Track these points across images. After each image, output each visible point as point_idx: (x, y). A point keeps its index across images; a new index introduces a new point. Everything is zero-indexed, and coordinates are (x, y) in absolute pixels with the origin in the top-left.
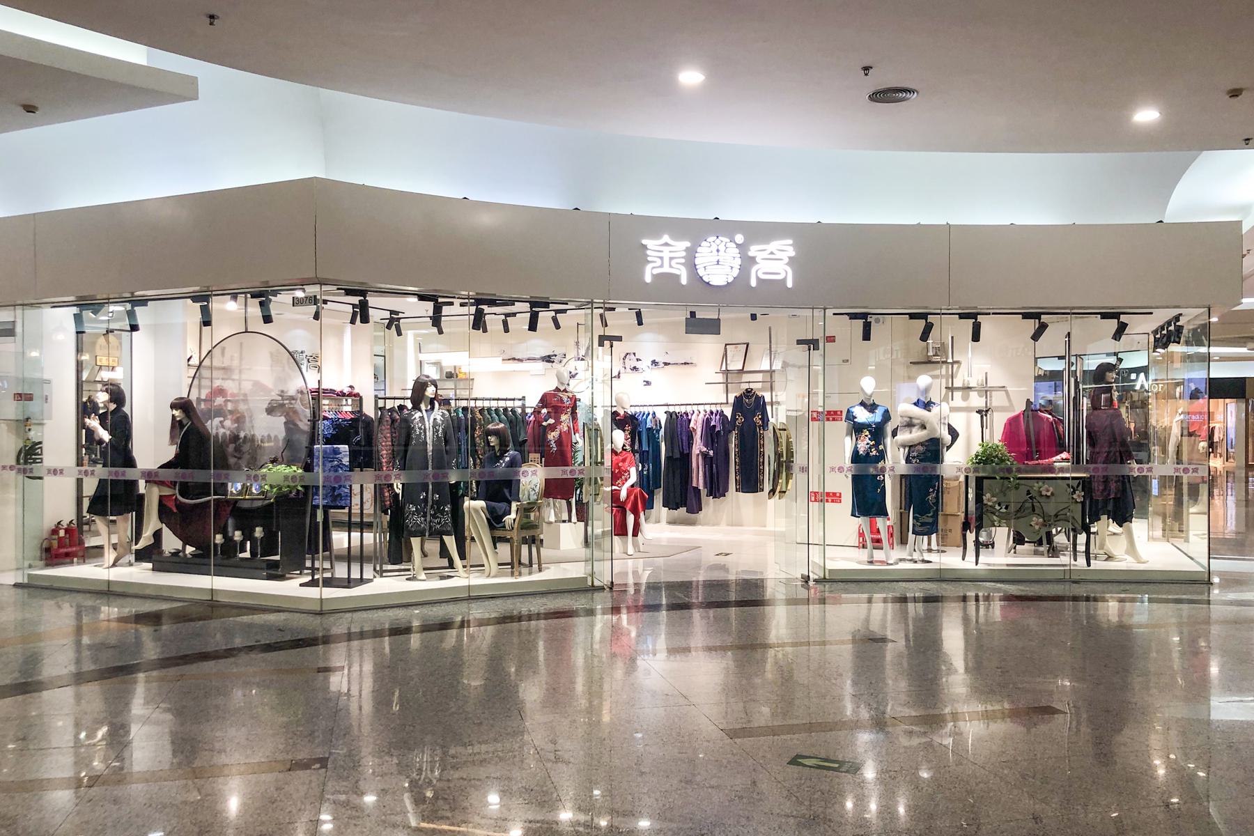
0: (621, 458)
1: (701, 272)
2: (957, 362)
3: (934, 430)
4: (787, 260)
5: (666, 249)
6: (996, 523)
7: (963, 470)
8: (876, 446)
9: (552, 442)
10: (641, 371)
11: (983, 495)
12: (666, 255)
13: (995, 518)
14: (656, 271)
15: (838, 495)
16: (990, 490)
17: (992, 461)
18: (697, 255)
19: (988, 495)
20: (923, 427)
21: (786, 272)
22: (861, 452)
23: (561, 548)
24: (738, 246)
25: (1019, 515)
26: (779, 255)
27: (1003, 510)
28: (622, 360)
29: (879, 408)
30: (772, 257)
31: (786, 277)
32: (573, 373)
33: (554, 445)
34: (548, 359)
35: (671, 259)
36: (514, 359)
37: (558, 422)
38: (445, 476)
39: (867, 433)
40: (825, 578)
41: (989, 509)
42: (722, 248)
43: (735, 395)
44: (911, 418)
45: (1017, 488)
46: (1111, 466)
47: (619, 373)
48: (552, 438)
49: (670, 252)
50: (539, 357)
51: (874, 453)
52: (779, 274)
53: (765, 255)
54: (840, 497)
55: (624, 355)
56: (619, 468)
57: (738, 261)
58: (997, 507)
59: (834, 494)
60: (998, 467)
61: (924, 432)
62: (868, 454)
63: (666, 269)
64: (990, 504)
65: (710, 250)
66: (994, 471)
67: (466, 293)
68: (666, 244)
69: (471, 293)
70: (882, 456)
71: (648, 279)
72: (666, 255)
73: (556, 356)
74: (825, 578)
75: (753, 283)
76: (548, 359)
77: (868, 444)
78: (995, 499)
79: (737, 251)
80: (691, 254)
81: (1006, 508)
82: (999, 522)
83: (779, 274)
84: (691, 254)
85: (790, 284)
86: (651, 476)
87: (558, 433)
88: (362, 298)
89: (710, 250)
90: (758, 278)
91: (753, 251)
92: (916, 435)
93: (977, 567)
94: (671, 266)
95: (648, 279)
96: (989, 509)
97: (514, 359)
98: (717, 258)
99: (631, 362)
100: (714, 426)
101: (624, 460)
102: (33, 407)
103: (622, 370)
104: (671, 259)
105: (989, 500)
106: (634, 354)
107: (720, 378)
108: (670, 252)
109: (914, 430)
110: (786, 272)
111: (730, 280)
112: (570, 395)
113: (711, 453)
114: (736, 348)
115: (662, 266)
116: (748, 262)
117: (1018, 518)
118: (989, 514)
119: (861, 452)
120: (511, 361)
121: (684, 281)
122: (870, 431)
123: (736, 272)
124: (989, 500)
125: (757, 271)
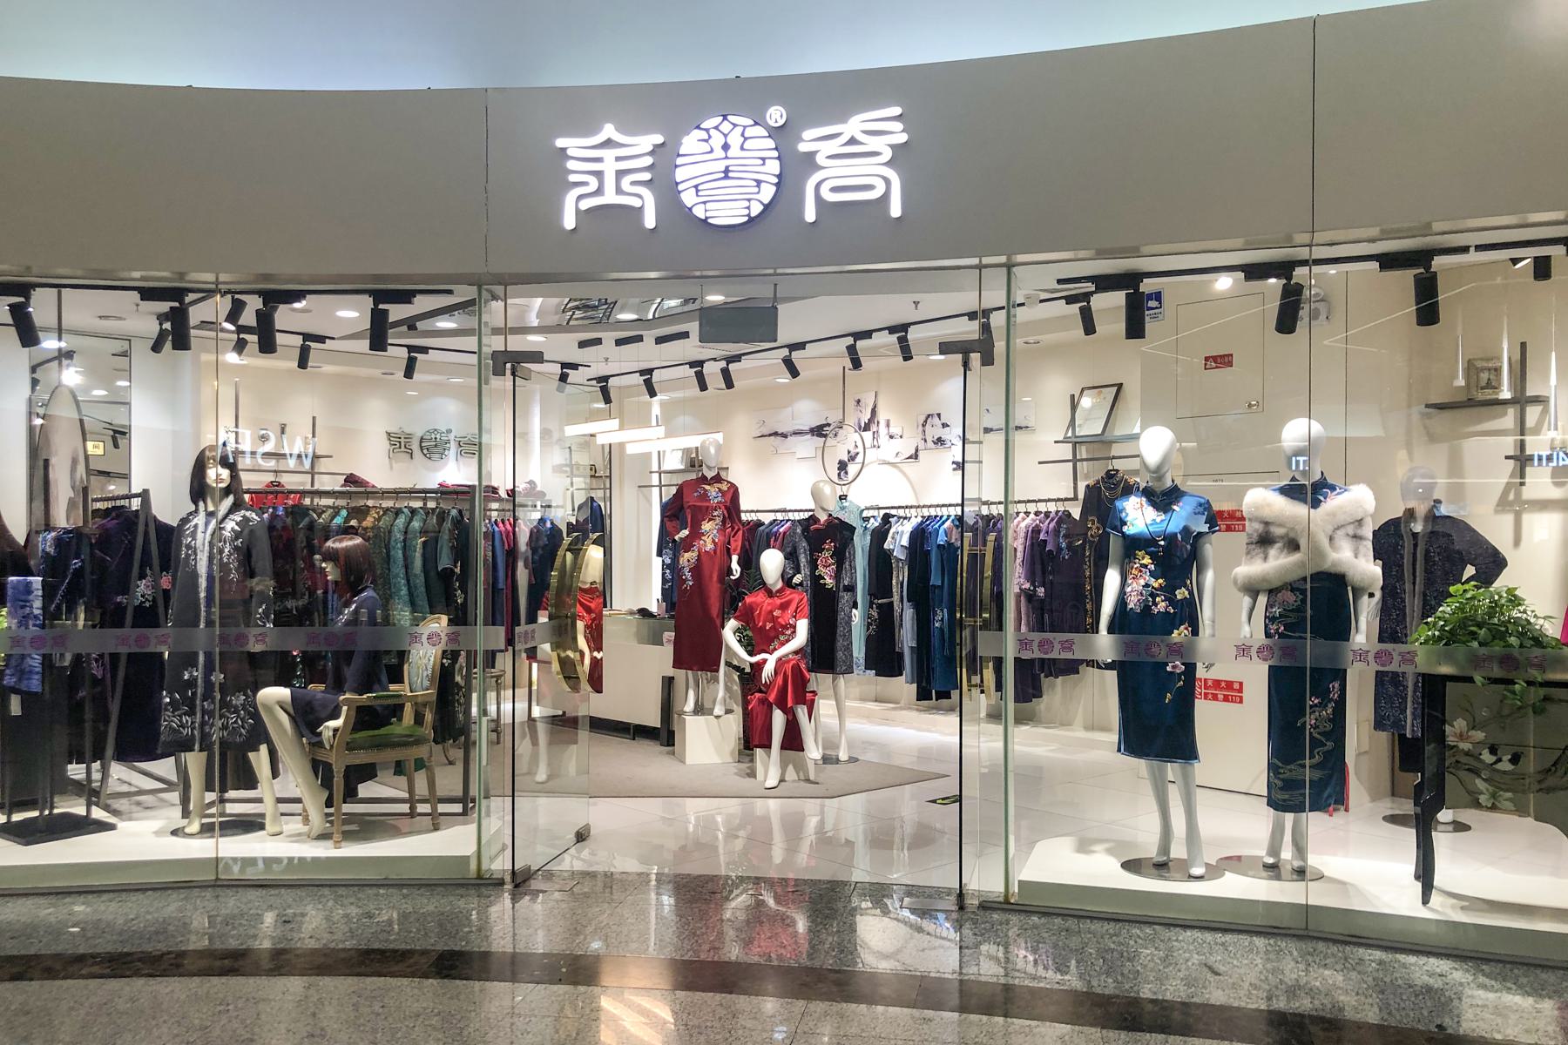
0: (778, 601)
1: (688, 198)
2: (1537, 400)
3: (1317, 552)
4: (887, 155)
5: (609, 154)
6: (1483, 799)
7: (1371, 657)
8: (1169, 591)
9: (686, 571)
10: (949, 444)
11: (1444, 722)
12: (609, 167)
13: (1480, 784)
14: (585, 204)
15: (1236, 686)
16: (1467, 711)
17: (1474, 635)
18: (776, 180)
19: (1460, 724)
20: (1293, 546)
21: (887, 181)
22: (1131, 605)
23: (688, 761)
24: (774, 133)
25: (1551, 781)
26: (873, 143)
27: (1505, 766)
28: (921, 428)
29: (1185, 498)
30: (853, 151)
31: (885, 197)
32: (852, 454)
33: (688, 575)
34: (819, 431)
35: (620, 174)
36: (775, 434)
37: (696, 534)
38: (241, 639)
39: (1147, 560)
40: (1007, 901)
41: (1464, 759)
42: (735, 139)
43: (1087, 483)
44: (1267, 524)
45: (1538, 711)
46: (644, 871)
47: (917, 450)
48: (686, 564)
49: (618, 159)
50: (807, 428)
51: (1162, 606)
52: (870, 187)
53: (833, 147)
54: (1240, 690)
55: (923, 418)
56: (774, 619)
57: (774, 167)
58: (1487, 757)
59: (1229, 685)
60: (1484, 651)
61: (1295, 557)
62: (1147, 609)
63: (610, 197)
64: (1465, 746)
65: (705, 147)
66: (1476, 661)
67: (210, 277)
68: (608, 143)
69: (223, 277)
70: (1188, 614)
71: (569, 222)
72: (609, 167)
73: (829, 425)
74: (1007, 901)
75: (810, 215)
76: (819, 431)
77: (1147, 585)
78: (1479, 735)
79: (771, 143)
80: (664, 157)
81: (1515, 759)
82: (1494, 796)
83: (870, 187)
84: (664, 157)
85: (896, 210)
86: (946, 630)
87: (695, 554)
88: (177, 304)
89: (705, 147)
90: (819, 200)
91: (808, 141)
92: (1275, 563)
93: (1423, 913)
94: (619, 191)
95: (569, 222)
96: (1464, 759)
97: (775, 434)
98: (721, 166)
99: (934, 431)
100: (1045, 541)
101: (784, 607)
102: (1278, 531)
103: (921, 445)
104: (620, 174)
105: (1461, 737)
106: (939, 415)
107: (1066, 451)
108: (618, 159)
109: (1273, 552)
110: (887, 181)
111: (756, 209)
112: (724, 487)
113: (1041, 591)
114: (1100, 393)
115: (599, 192)
116: (795, 167)
117: (1549, 790)
118: (1462, 774)
119: (1131, 605)
120: (772, 438)
121: (650, 221)
122: (1153, 556)
123: (768, 193)
124: (1461, 737)
125: (818, 186)
